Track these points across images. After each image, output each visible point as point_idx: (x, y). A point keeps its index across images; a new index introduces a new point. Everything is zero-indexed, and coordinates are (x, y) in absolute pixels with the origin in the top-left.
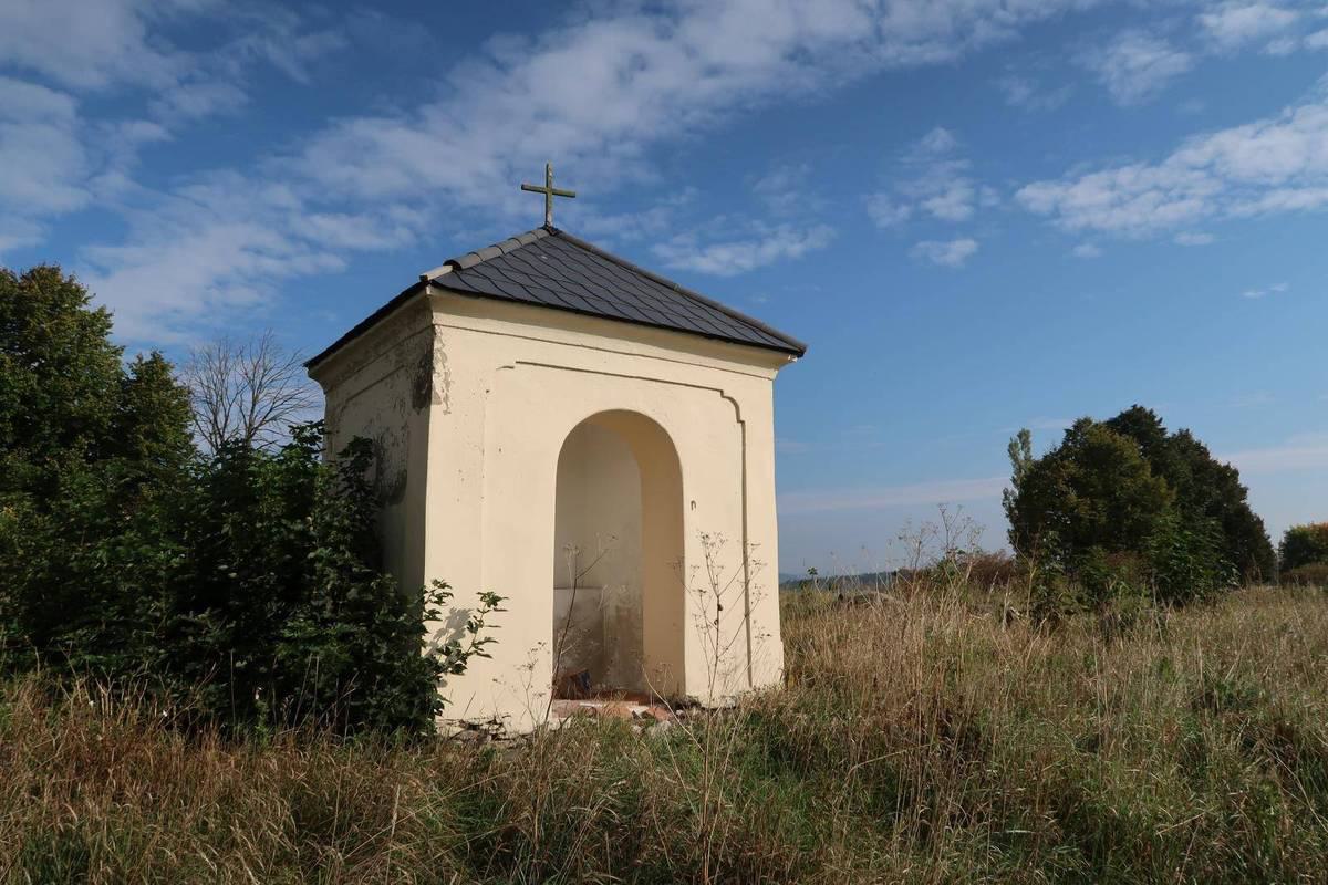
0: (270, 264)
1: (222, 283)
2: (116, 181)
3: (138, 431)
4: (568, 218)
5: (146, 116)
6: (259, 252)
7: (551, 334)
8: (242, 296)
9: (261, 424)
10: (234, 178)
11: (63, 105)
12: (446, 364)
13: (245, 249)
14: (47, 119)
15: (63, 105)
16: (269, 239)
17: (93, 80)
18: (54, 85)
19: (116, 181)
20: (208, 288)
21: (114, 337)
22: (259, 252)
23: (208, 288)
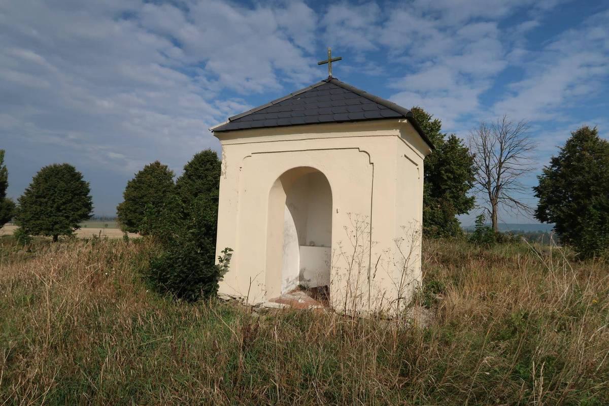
0: (597, 70)
1: (571, 86)
2: (519, 52)
3: (442, 170)
4: (345, 74)
5: (527, 18)
6: (589, 66)
7: (304, 136)
8: (582, 90)
9: (504, 161)
10: (572, 32)
11: (491, 27)
12: (226, 159)
13: (581, 66)
14: (486, 35)
15: (491, 27)
16: (595, 57)
17: (502, 11)
18: (488, 20)
19: (519, 52)
20: (565, 90)
21: (442, 131)
22: (589, 66)
23: (565, 90)
